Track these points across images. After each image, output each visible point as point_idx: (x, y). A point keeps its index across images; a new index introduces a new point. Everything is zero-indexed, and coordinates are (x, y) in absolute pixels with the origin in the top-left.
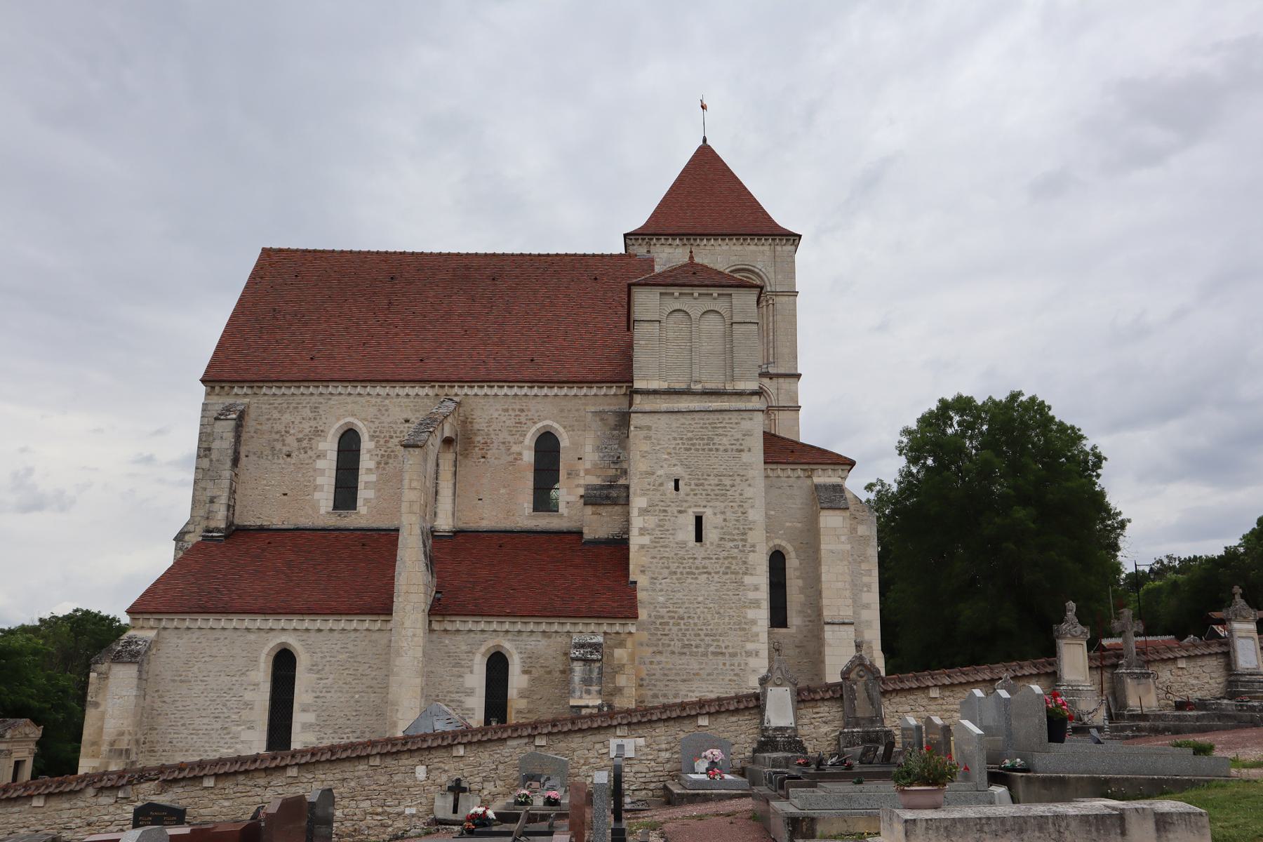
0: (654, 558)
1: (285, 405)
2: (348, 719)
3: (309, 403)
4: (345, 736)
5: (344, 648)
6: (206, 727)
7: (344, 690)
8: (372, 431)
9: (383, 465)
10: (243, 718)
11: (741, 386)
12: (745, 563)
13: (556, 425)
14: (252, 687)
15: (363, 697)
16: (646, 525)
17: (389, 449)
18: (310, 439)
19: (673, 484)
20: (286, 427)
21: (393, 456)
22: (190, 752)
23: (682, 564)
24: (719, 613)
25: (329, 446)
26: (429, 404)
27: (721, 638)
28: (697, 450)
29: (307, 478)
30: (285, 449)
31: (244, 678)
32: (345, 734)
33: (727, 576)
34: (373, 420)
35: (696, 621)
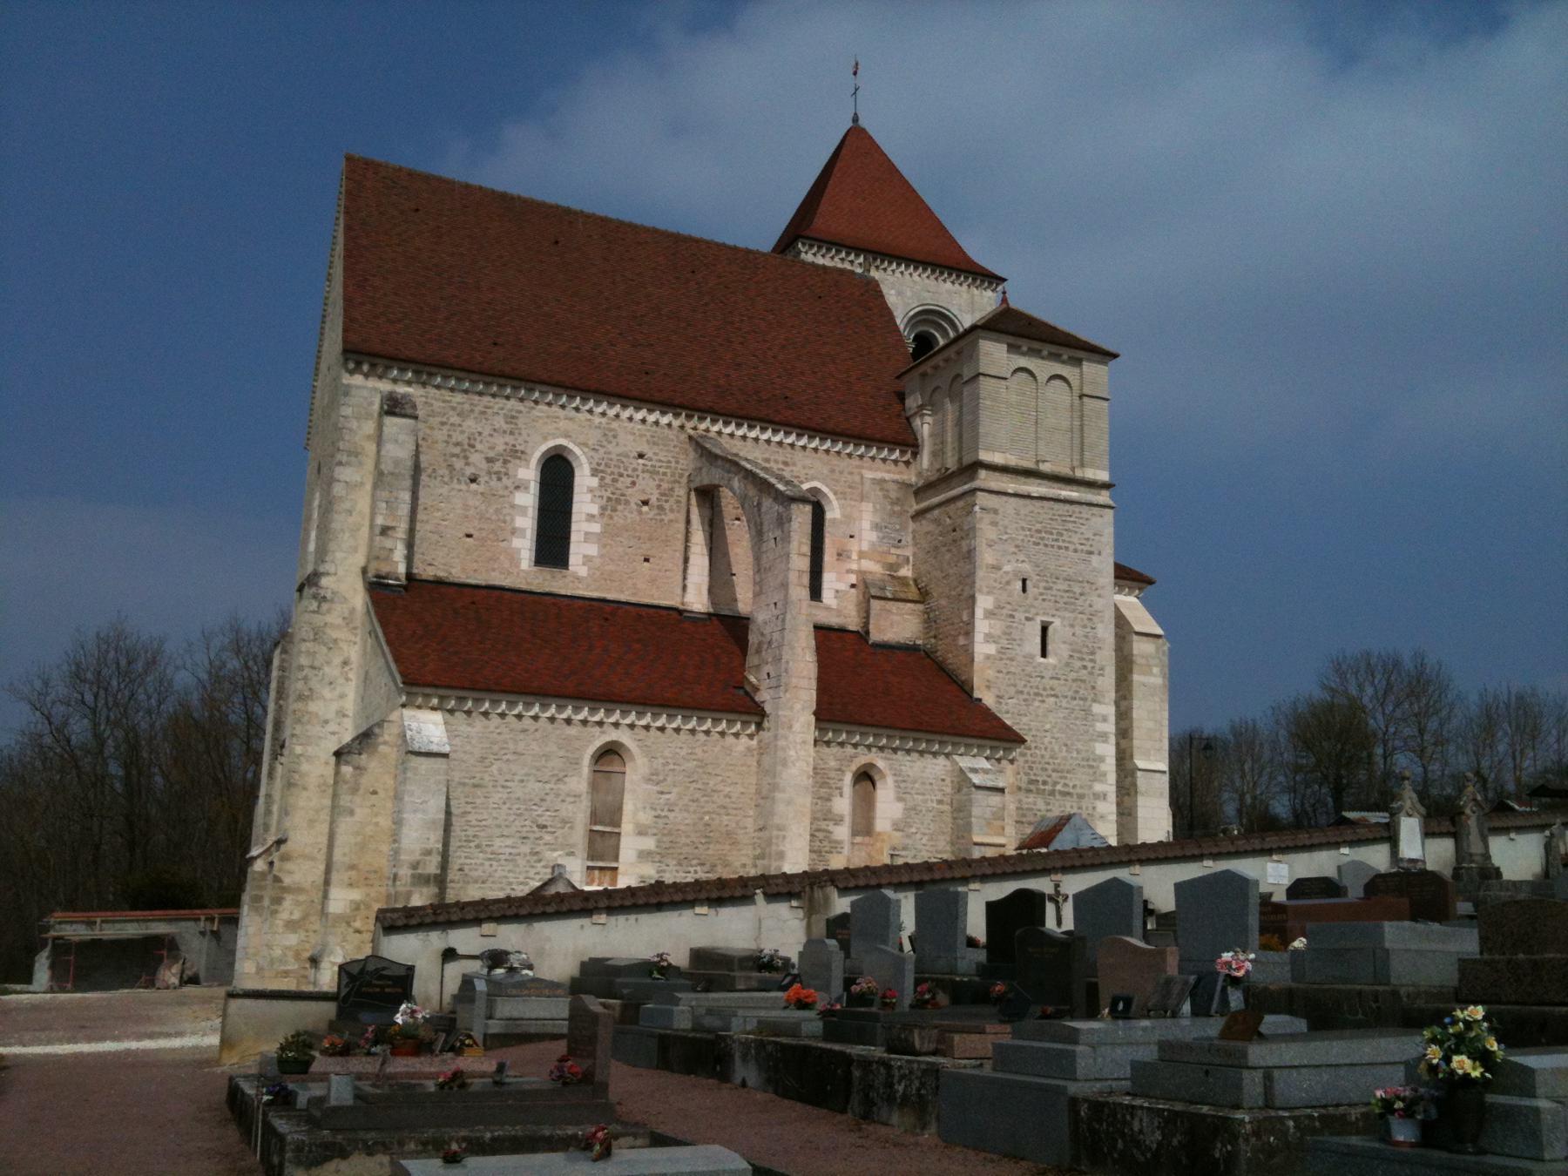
0: (999, 672)
1: (467, 407)
2: (696, 848)
3: (502, 409)
4: (692, 869)
5: (691, 754)
6: (509, 850)
7: (692, 809)
8: (594, 463)
9: (609, 512)
10: (560, 840)
11: (1090, 474)
12: (1093, 688)
13: (825, 489)
14: (572, 799)
15: (713, 819)
16: (992, 631)
17: (618, 492)
18: (505, 462)
19: (1019, 584)
20: (469, 439)
21: (623, 502)
22: (488, 885)
23: (1029, 682)
24: (1066, 745)
25: (529, 473)
26: (672, 437)
27: (1068, 775)
28: (1046, 545)
29: (502, 518)
30: (469, 471)
31: (561, 786)
32: (692, 866)
33: (1075, 702)
34: (597, 447)
35: (1043, 752)
